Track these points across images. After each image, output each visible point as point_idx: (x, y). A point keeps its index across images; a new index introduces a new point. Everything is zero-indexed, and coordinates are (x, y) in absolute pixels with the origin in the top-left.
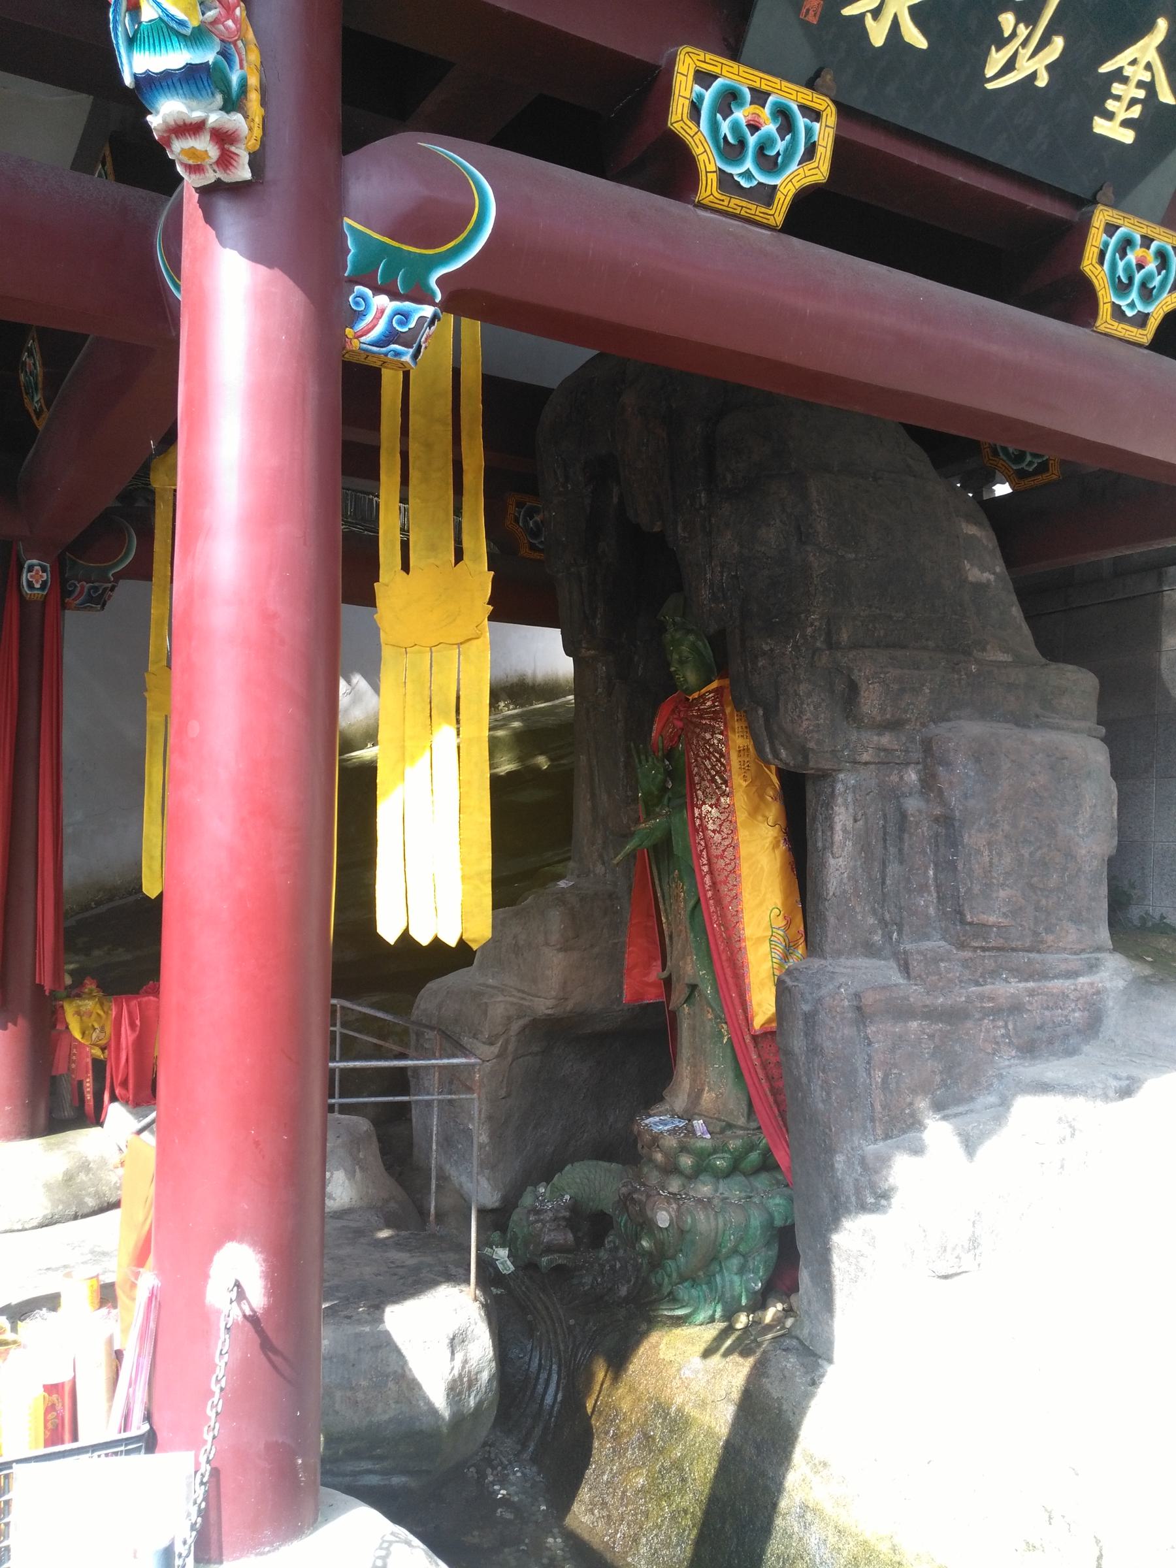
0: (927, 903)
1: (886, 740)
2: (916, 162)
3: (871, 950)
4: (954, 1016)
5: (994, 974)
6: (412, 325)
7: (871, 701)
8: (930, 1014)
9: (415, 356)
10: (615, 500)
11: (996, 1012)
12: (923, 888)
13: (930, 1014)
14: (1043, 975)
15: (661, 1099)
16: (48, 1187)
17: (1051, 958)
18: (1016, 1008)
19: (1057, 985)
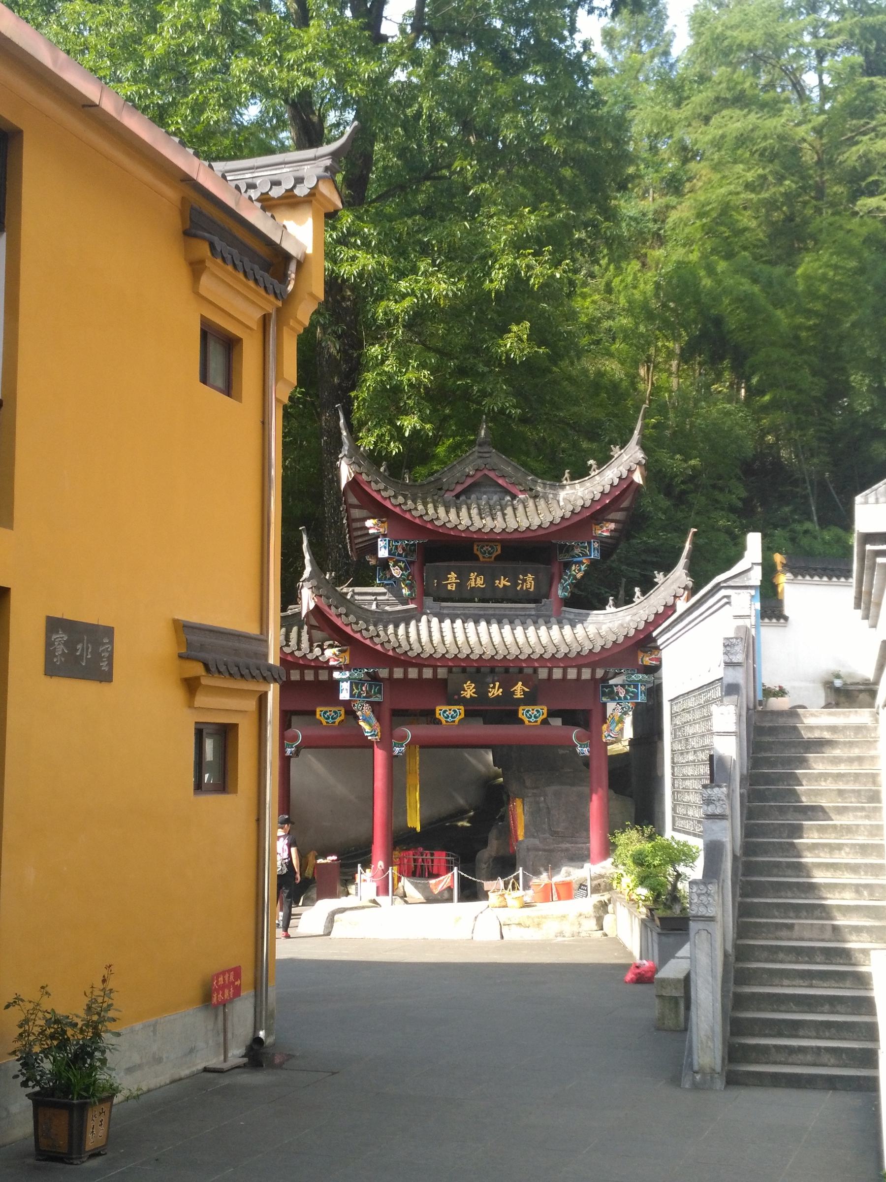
0: (546, 826)
1: (535, 791)
2: (599, 507)
3: (534, 837)
4: (550, 851)
5: (562, 842)
6: (377, 432)
7: (528, 783)
8: (545, 850)
9: (250, 198)
10: (75, 1115)
11: (562, 851)
12: (544, 823)
13: (545, 850)
14: (576, 843)
15: (426, 464)
16: (668, 17)
17: (579, 839)
18: (567, 850)
19: (580, 845)
